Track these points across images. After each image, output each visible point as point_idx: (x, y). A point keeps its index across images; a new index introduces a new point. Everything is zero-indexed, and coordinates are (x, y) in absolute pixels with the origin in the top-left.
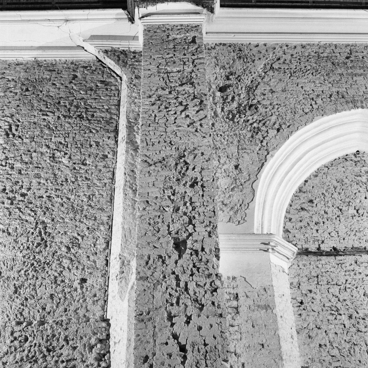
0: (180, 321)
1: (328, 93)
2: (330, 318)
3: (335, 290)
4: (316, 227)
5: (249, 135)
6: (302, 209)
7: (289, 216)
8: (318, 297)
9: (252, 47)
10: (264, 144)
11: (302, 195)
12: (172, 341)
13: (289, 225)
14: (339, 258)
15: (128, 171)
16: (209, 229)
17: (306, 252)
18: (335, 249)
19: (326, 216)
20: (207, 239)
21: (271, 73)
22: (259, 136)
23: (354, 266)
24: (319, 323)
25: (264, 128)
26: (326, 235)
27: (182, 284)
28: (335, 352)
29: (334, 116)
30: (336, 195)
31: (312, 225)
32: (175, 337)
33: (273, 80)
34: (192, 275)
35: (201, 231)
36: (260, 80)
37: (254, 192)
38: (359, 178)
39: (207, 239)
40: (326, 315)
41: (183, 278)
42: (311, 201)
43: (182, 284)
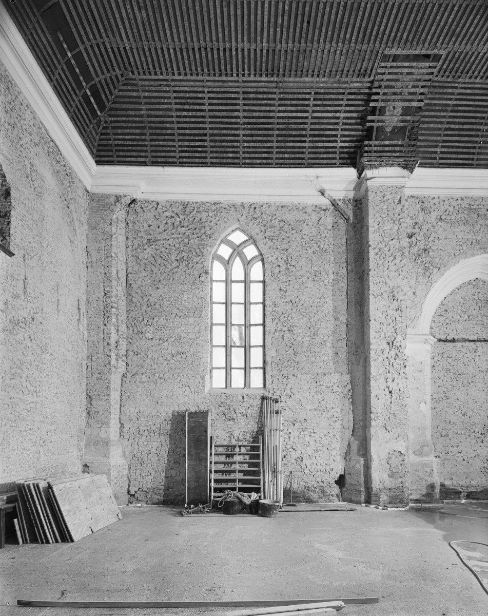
0: (390, 380)
1: (470, 240)
2: (446, 374)
3: (450, 360)
4: (446, 326)
5: (423, 272)
6: (441, 315)
7: (434, 319)
8: (441, 363)
9: (430, 199)
10: (430, 278)
11: (442, 306)
12: (386, 389)
13: (433, 325)
14: (455, 344)
15: (356, 293)
16: (403, 336)
17: (440, 340)
18: (454, 339)
19: (452, 320)
20: (402, 341)
21: (439, 223)
22: (428, 273)
23: (461, 349)
24: (440, 376)
25: (431, 268)
26: (450, 331)
27: (391, 364)
28: (445, 390)
29: (472, 259)
30: (459, 307)
31: (445, 324)
32: (388, 387)
33: (440, 229)
34: (395, 359)
35: (400, 337)
36: (433, 230)
37: (421, 310)
38: (474, 296)
39: (402, 341)
40: (443, 373)
41: (392, 360)
42: (446, 311)
43: (391, 364)
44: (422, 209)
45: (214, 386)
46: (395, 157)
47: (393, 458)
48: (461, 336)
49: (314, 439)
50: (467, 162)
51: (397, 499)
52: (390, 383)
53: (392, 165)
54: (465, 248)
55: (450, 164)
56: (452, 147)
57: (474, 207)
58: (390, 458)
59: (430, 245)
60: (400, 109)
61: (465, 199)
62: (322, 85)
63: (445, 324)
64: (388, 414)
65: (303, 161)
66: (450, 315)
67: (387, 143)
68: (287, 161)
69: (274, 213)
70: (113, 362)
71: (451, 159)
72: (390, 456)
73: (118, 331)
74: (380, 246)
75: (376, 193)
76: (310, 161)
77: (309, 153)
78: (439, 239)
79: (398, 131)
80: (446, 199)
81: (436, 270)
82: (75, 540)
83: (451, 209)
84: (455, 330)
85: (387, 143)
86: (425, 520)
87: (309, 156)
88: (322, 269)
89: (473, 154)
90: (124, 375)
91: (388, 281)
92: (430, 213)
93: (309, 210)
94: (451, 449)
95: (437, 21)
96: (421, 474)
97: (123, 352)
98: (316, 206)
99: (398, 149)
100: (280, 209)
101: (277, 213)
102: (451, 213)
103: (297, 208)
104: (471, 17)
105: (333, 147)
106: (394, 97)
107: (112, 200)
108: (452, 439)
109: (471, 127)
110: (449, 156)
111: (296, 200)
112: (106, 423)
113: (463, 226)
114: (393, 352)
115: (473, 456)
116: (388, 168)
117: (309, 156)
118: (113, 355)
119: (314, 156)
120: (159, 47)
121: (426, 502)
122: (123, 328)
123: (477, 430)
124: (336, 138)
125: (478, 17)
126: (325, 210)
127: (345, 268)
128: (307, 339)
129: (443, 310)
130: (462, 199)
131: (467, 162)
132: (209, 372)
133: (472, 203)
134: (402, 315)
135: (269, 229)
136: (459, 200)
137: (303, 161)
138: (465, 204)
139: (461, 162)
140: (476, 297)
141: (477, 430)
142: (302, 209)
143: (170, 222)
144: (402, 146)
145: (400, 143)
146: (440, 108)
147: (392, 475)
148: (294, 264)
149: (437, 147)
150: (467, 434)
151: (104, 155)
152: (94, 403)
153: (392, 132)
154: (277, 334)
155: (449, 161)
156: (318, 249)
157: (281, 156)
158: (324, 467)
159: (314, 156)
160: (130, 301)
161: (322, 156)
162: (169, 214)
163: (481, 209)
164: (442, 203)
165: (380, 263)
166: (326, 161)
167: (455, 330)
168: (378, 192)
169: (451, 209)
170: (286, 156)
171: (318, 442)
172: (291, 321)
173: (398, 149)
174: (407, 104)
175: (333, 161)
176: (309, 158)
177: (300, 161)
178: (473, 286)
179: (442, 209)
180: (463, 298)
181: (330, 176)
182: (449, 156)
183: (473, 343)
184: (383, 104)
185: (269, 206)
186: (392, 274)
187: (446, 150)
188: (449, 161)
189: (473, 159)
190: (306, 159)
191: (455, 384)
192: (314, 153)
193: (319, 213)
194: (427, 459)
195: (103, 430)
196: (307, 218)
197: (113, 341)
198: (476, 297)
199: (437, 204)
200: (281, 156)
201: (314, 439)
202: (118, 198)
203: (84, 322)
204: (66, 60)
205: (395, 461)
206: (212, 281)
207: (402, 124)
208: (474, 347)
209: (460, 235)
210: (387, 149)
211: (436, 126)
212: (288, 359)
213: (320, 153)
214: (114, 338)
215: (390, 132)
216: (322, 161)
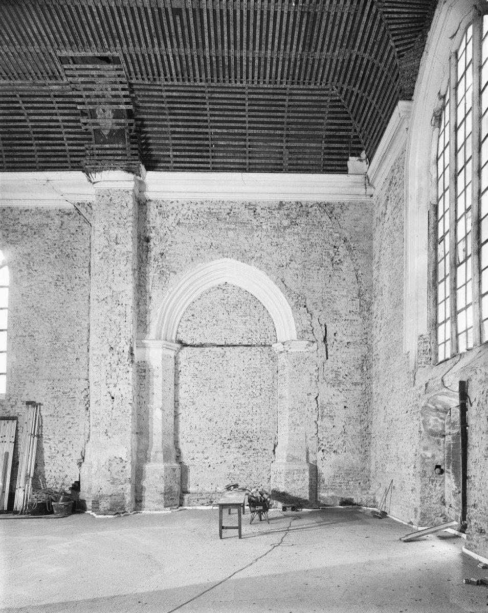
2: (192, 379)
3: (196, 365)
9: (168, 203)
10: (166, 283)
12: (109, 395)
14: (203, 349)
21: (177, 227)
26: (198, 336)
28: (191, 395)
46: (116, 160)
47: (114, 464)
48: (209, 341)
49: (49, 445)
50: (202, 165)
51: (118, 506)
52: (112, 389)
53: (115, 169)
55: (185, 168)
56: (185, 151)
57: (214, 211)
58: (110, 465)
60: (111, 112)
61: (205, 203)
62: (7, 87)
63: (192, 329)
64: (110, 420)
65: (34, 165)
66: (198, 320)
67: (107, 146)
68: (18, 165)
69: (17, 217)
71: (185, 162)
72: (111, 462)
74: (106, 250)
75: (103, 196)
76: (41, 165)
77: (39, 156)
79: (116, 135)
80: (185, 203)
84: (202, 335)
85: (107, 146)
86: (359, 524)
87: (39, 159)
88: (64, 273)
89: (208, 157)
91: (113, 286)
92: (168, 216)
93: (52, 214)
95: (85, 23)
98: (60, 210)
99: (120, 152)
100: (23, 213)
101: (20, 218)
102: (190, 217)
103: (39, 211)
104: (43, 18)
105: (62, 151)
106: (97, 100)
108: (198, 445)
109: (197, 130)
110: (182, 160)
111: (40, 204)
113: (201, 230)
116: (111, 171)
117: (39, 159)
119: (44, 159)
120: (131, 48)
123: (223, 436)
124: (62, 142)
125: (57, 18)
126: (68, 214)
127: (88, 272)
128: (49, 344)
130: (202, 203)
131: (202, 165)
133: (212, 207)
134: (127, 320)
135: (11, 234)
136: (199, 203)
137: (34, 165)
139: (196, 165)
140: (225, 302)
141: (223, 436)
142: (47, 214)
144: (124, 149)
145: (121, 146)
146: (156, 111)
148: (36, 269)
149: (168, 150)
150: (214, 440)
153: (110, 135)
154: (18, 339)
155: (183, 165)
156: (60, 253)
157: (11, 159)
158: (58, 474)
159: (44, 159)
161: (52, 159)
163: (221, 212)
164: (180, 207)
165: (105, 268)
166: (57, 165)
167: (202, 335)
168: (105, 196)
169: (190, 213)
170: (16, 159)
171: (53, 449)
172: (32, 326)
173: (120, 152)
174: (115, 107)
175: (65, 165)
176: (39, 162)
177: (30, 165)
178: (221, 290)
180: (212, 303)
181: (61, 180)
182: (182, 160)
184: (91, 107)
185: (12, 211)
187: (178, 153)
188: (183, 165)
189: (208, 163)
190: (37, 162)
191: (202, 389)
192: (43, 156)
193: (62, 217)
196: (50, 222)
198: (225, 302)
199: (176, 208)
200: (11, 159)
201: (49, 445)
204: (71, 61)
207: (118, 127)
208: (222, 351)
209: (198, 240)
210: (109, 152)
211: (160, 129)
212: (28, 365)
213: (50, 156)
215: (108, 135)
216: (53, 165)
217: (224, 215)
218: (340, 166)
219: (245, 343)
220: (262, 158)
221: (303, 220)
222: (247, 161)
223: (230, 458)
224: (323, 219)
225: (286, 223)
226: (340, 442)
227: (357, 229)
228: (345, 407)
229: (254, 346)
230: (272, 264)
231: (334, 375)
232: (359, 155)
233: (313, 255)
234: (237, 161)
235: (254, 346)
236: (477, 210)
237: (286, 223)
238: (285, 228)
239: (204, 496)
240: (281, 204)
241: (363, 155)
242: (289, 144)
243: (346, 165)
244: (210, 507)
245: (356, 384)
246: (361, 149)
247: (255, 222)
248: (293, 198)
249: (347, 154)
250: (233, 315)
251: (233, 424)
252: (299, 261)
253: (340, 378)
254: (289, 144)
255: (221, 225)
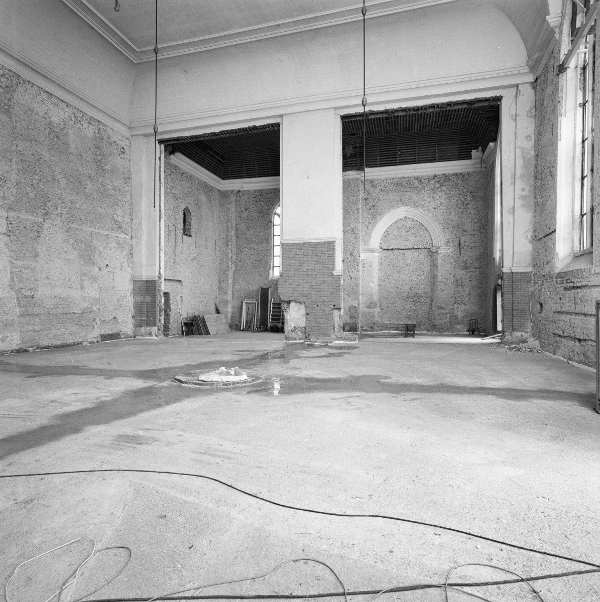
32: (350, 275)
41: (352, 263)
44: (372, 186)
45: (274, 275)
52: (351, 274)
54: (394, 204)
59: (376, 203)
70: (230, 265)
73: (232, 251)
78: (380, 200)
81: (378, 216)
82: (211, 333)
83: (387, 185)
90: (234, 272)
94: (390, 305)
96: (368, 317)
97: (235, 261)
107: (230, 193)
112: (226, 293)
114: (352, 259)
115: (402, 309)
118: (230, 262)
121: (370, 331)
122: (234, 250)
129: (386, 235)
130: (393, 179)
132: (272, 269)
138: (394, 181)
143: (255, 199)
144: (356, 161)
147: (351, 317)
151: (225, 175)
152: (221, 284)
153: (350, 156)
160: (237, 237)
162: (254, 196)
169: (387, 185)
179: (383, 185)
183: (402, 251)
186: (353, 221)
194: (372, 310)
195: (225, 296)
197: (230, 256)
202: (232, 191)
203: (218, 248)
205: (352, 311)
206: (274, 225)
214: (230, 255)
217: (405, 184)
218: (468, 154)
219: (416, 247)
220: (424, 155)
221: (447, 183)
222: (417, 157)
223: (408, 307)
224: (458, 182)
225: (437, 186)
226: (467, 299)
227: (478, 186)
228: (470, 281)
229: (420, 249)
230: (430, 208)
231: (464, 264)
232: (478, 149)
233: (453, 201)
234: (411, 157)
235: (420, 249)
236: (264, 596)
237: (437, 186)
238: (437, 188)
239: (393, 326)
240: (435, 176)
241: (480, 148)
242: (438, 148)
243: (471, 154)
244: (397, 332)
245: (476, 268)
246: (479, 146)
247: (421, 187)
248: (441, 173)
249: (471, 149)
250: (410, 234)
251: (409, 289)
252: (444, 204)
253: (467, 265)
254: (438, 148)
255: (403, 189)
